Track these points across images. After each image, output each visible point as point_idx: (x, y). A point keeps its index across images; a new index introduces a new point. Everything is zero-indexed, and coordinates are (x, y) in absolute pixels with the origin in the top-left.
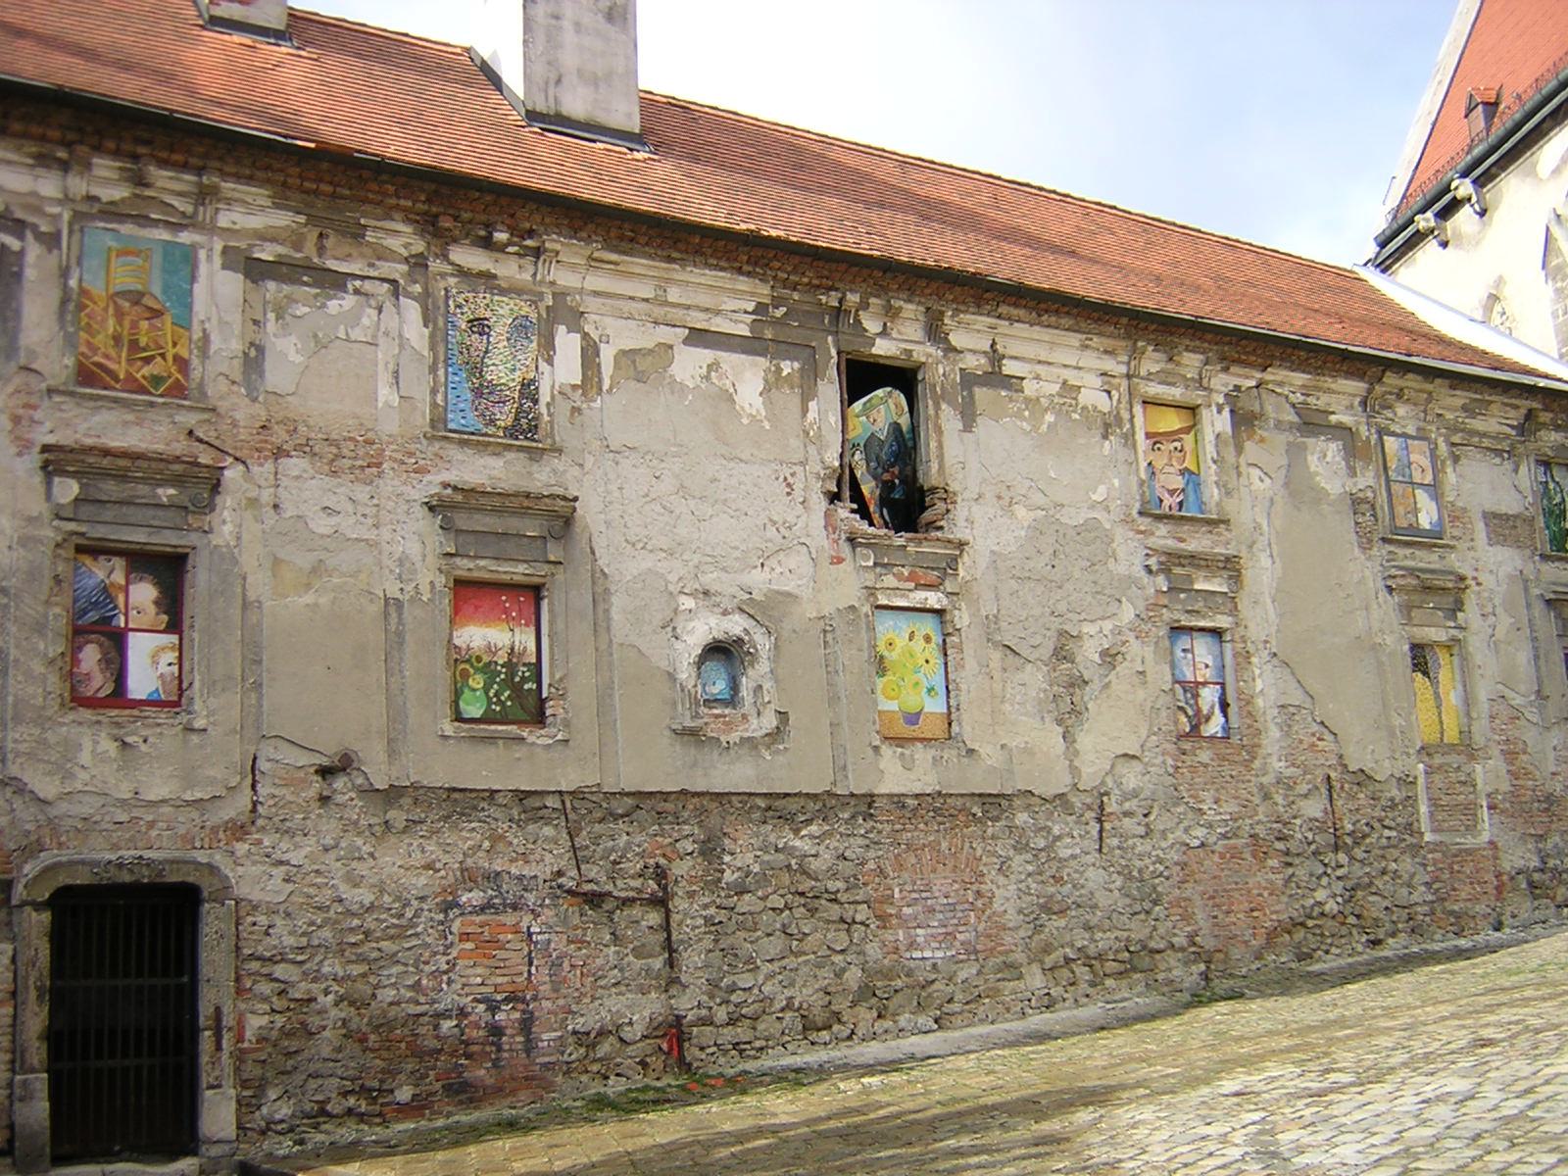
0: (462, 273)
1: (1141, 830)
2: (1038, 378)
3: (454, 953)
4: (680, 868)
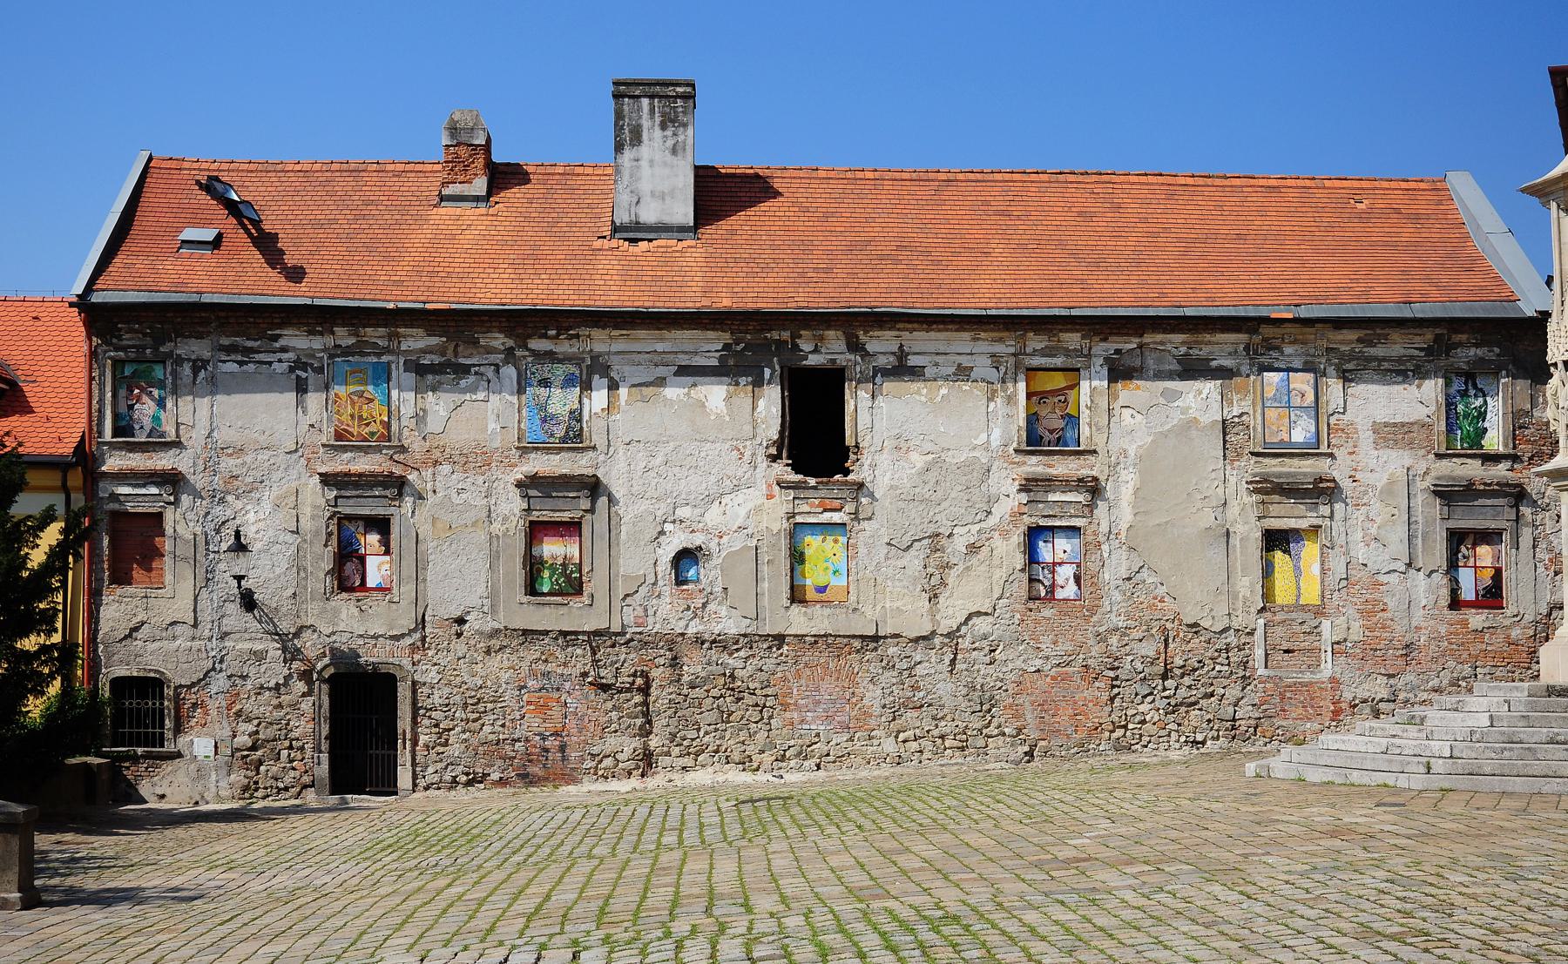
0: (534, 353)
1: (987, 659)
2: (937, 364)
3: (524, 710)
4: (655, 673)
